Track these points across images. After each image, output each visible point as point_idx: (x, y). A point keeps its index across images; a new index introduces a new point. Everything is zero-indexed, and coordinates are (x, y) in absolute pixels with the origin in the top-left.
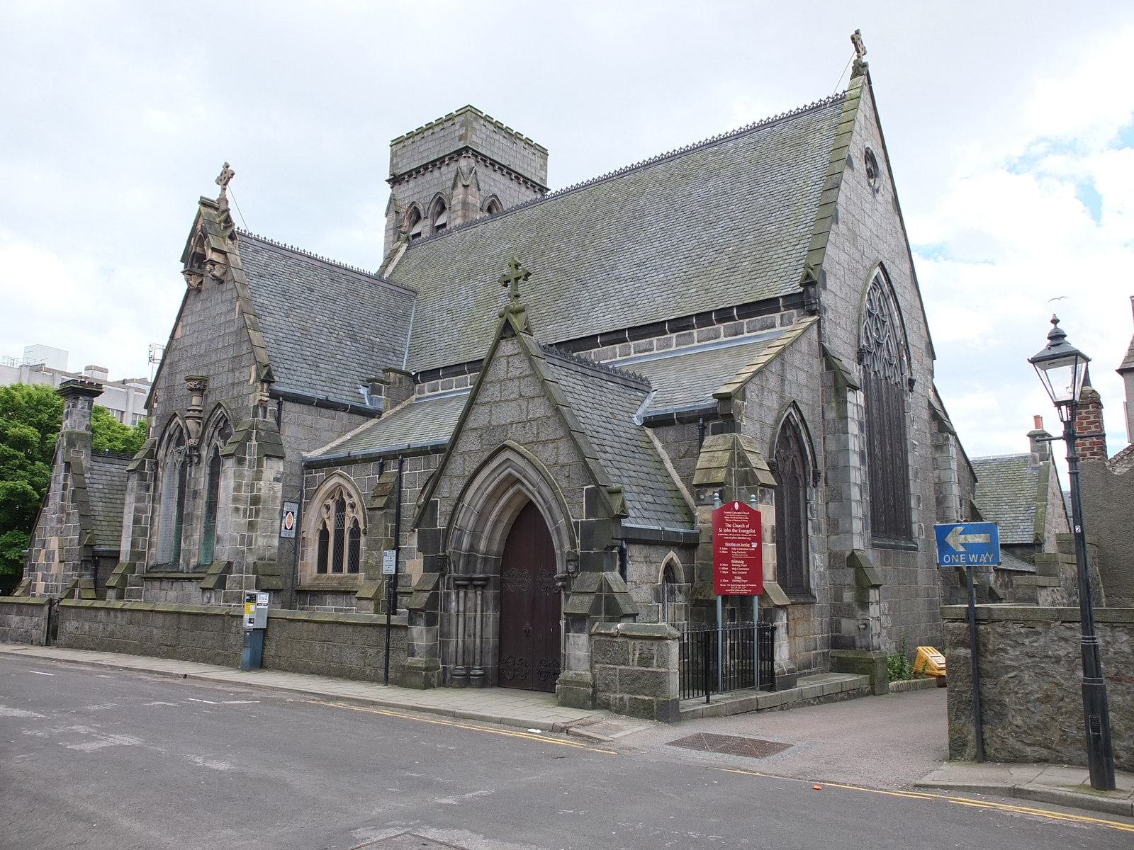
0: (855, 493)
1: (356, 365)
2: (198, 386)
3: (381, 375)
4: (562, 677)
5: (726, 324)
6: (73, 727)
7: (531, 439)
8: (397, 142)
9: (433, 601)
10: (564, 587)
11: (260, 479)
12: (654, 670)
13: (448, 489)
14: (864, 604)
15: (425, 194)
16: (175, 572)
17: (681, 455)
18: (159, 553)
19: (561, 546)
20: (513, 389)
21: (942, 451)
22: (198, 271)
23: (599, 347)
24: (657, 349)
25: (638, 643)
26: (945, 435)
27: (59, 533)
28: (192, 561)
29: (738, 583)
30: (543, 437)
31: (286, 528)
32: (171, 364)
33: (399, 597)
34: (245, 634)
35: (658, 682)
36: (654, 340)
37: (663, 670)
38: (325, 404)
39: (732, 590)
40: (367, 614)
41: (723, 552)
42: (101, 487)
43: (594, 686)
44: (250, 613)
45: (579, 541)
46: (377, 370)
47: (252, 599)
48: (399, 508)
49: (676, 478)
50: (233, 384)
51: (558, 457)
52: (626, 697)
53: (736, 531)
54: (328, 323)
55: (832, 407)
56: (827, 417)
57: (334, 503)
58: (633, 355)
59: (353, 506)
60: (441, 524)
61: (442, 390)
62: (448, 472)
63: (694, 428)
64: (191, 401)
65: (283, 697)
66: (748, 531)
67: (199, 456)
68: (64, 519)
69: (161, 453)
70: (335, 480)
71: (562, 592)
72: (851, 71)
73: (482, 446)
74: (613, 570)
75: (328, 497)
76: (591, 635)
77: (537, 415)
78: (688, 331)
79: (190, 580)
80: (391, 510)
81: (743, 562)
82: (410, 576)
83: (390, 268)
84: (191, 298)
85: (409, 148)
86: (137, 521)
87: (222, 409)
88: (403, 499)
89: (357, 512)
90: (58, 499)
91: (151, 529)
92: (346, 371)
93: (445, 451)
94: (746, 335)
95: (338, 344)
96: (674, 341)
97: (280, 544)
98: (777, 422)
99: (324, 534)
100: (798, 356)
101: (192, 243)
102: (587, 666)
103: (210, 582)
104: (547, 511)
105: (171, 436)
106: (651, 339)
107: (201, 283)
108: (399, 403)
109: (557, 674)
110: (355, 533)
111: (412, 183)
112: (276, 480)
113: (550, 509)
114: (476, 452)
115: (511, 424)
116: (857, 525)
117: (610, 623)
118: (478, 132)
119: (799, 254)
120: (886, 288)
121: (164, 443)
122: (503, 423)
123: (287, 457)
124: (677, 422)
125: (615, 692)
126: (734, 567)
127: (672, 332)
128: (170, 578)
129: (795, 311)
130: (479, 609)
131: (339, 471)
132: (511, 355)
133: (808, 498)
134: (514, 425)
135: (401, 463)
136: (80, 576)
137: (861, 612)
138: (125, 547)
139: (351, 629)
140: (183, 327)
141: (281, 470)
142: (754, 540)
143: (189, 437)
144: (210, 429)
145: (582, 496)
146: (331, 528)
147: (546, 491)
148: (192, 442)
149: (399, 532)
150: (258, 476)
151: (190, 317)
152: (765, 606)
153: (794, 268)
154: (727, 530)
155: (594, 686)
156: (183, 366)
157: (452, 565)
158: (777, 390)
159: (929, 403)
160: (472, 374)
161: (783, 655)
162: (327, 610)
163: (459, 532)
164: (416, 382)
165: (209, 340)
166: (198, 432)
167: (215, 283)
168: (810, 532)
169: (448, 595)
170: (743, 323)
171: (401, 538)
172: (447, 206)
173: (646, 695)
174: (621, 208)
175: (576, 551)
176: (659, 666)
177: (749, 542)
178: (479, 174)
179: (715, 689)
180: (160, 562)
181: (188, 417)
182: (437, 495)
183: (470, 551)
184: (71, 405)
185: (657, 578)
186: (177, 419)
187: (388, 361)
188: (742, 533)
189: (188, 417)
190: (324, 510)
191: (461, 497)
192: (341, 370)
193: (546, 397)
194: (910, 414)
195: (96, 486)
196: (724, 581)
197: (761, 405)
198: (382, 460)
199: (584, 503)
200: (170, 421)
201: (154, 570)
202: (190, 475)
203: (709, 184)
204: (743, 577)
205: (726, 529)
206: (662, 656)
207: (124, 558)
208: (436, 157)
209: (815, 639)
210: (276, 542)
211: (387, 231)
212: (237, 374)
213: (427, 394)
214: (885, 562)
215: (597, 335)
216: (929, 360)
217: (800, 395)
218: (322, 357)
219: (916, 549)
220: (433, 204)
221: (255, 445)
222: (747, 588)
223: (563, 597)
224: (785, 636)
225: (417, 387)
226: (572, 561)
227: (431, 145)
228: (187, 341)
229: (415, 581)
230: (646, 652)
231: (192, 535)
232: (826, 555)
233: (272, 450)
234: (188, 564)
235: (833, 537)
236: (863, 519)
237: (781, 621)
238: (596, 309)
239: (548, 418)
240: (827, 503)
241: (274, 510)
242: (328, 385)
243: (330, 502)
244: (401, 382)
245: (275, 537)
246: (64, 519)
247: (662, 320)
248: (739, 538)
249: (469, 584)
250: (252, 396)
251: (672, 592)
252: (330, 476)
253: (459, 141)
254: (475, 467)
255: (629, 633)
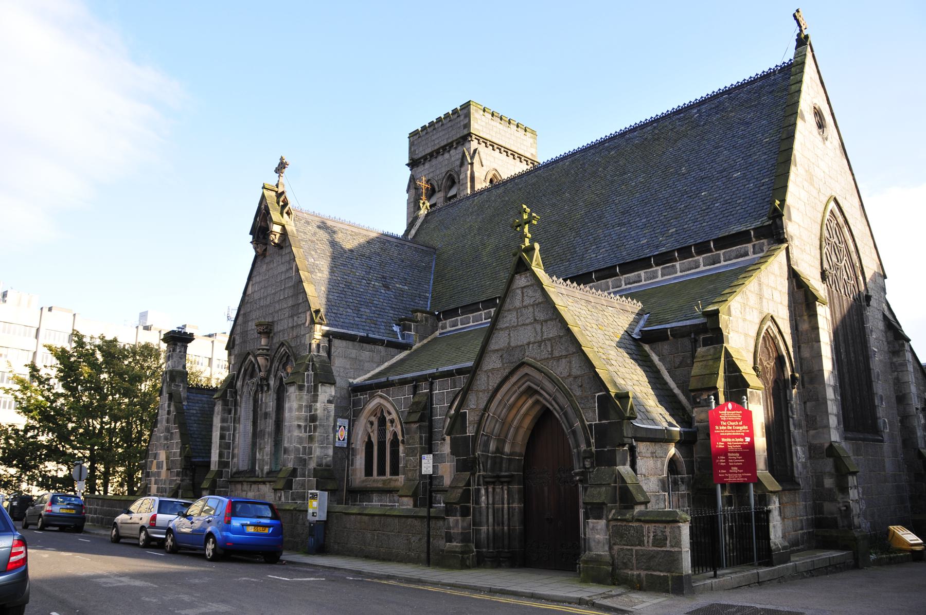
0: (830, 394)
1: (389, 308)
2: (265, 330)
3: (410, 315)
4: (584, 557)
5: (705, 255)
6: (180, 596)
7: (546, 356)
8: (414, 135)
9: (466, 495)
10: (581, 481)
11: (316, 401)
12: (668, 549)
13: (475, 402)
14: (844, 489)
15: (438, 172)
16: (252, 477)
17: (676, 366)
18: (240, 461)
19: (578, 446)
20: (529, 313)
21: (899, 356)
22: (264, 241)
23: (594, 282)
24: (645, 281)
25: (652, 527)
26: (901, 342)
27: (167, 448)
28: (265, 468)
29: (735, 473)
30: (556, 354)
31: (339, 439)
32: (244, 314)
33: (434, 494)
34: (310, 525)
35: (673, 559)
36: (642, 273)
37: (676, 549)
38: (366, 340)
39: (730, 479)
40: (407, 504)
41: (720, 446)
42: (195, 412)
43: (613, 564)
44: (314, 508)
45: (594, 441)
46: (407, 312)
47: (314, 496)
48: (431, 421)
49: (672, 384)
50: (293, 327)
51: (571, 370)
52: (643, 573)
53: (731, 428)
54: (365, 276)
55: (804, 320)
56: (800, 329)
57: (377, 420)
58: (624, 287)
59: (392, 421)
60: (470, 432)
61: (461, 325)
62: (475, 388)
63: (686, 342)
64: (261, 342)
65: (344, 576)
66: (741, 428)
67: (268, 385)
68: (169, 437)
69: (239, 384)
70: (377, 401)
71: (579, 485)
72: (795, 43)
73: (503, 364)
74: (624, 464)
75: (371, 414)
76: (608, 521)
77: (551, 335)
78: (671, 264)
79: (264, 483)
80: (424, 423)
81: (738, 455)
82: (442, 477)
83: (413, 232)
84: (259, 263)
85: (423, 138)
86: (222, 437)
87: (285, 347)
88: (434, 414)
89: (396, 426)
90: (164, 423)
91: (233, 443)
92: (381, 313)
93: (472, 373)
94: (723, 263)
95: (375, 293)
96: (660, 273)
97: (335, 453)
98: (758, 334)
99: (369, 445)
100: (772, 277)
101: (258, 220)
102: (607, 548)
103: (280, 485)
104: (563, 416)
105: (246, 371)
106: (639, 272)
107: (265, 250)
108: (426, 337)
109: (577, 556)
110: (395, 443)
111: (427, 165)
112: (329, 402)
113: (565, 414)
114: (498, 370)
115: (528, 344)
116: (833, 421)
117: (624, 510)
118: (479, 121)
119: (764, 194)
120: (841, 220)
121: (241, 376)
122: (521, 344)
123: (337, 384)
124: (671, 338)
125: (632, 570)
126: (730, 459)
127: (657, 265)
128: (249, 482)
129: (765, 241)
130: (505, 502)
131: (380, 393)
132: (525, 287)
133: (788, 399)
134: (531, 346)
135: (432, 384)
136: (182, 480)
137: (841, 496)
138: (215, 457)
139: (396, 520)
140: (253, 285)
141: (333, 394)
142: (747, 435)
143: (260, 371)
144: (276, 364)
145: (595, 403)
146: (375, 440)
147: (562, 400)
148: (262, 374)
149: (431, 441)
150: (315, 398)
151: (257, 277)
152: (760, 492)
153: (761, 205)
154: (723, 428)
155: (613, 564)
156: (254, 315)
157: (481, 465)
158: (757, 307)
159: (884, 315)
160: (486, 311)
161: (777, 533)
162: (376, 504)
163: (486, 438)
164: (439, 320)
165: (273, 294)
166: (266, 366)
167: (276, 249)
168: (792, 428)
169: (478, 491)
170: (719, 254)
171: (433, 446)
172: (456, 181)
173: (661, 571)
174: (604, 169)
175: (591, 449)
176: (672, 546)
177: (743, 437)
178: (481, 154)
179: (720, 566)
180: (241, 469)
181: (259, 355)
182: (465, 407)
183: (495, 453)
184: (171, 349)
185: (662, 470)
186: (251, 357)
187: (416, 304)
188: (736, 430)
189: (259, 355)
190: (369, 426)
191: (486, 408)
192: (378, 312)
193: (558, 320)
194: (869, 325)
195: (192, 411)
196: (723, 471)
197: (744, 320)
198: (415, 383)
199: (597, 408)
200: (245, 359)
201: (237, 476)
202: (262, 400)
203: (679, 144)
204: (739, 467)
205: (722, 426)
206: (675, 538)
207: (214, 467)
208: (445, 143)
209: (801, 521)
210: (330, 452)
211: (408, 203)
212: (295, 318)
213: (449, 329)
214: (857, 452)
215: (592, 272)
216: (881, 279)
217: (776, 311)
218: (362, 303)
219: (882, 441)
220: (444, 180)
221: (311, 374)
222: (743, 477)
223: (581, 489)
224: (779, 518)
225: (440, 324)
226: (588, 458)
227: (441, 134)
228: (256, 296)
229: (447, 481)
230: (660, 534)
231: (265, 448)
232: (807, 448)
233: (325, 376)
234: (262, 470)
235: (812, 432)
236: (837, 416)
237: (774, 506)
238: (589, 251)
239: (560, 337)
240: (805, 403)
241: (329, 426)
242: (368, 325)
243: (373, 419)
244: (426, 320)
245: (329, 448)
246: (169, 437)
247: (648, 255)
248: (734, 434)
249: (495, 480)
250: (307, 335)
251: (675, 483)
252: (372, 397)
253: (464, 129)
254: (498, 382)
255: (643, 518)
